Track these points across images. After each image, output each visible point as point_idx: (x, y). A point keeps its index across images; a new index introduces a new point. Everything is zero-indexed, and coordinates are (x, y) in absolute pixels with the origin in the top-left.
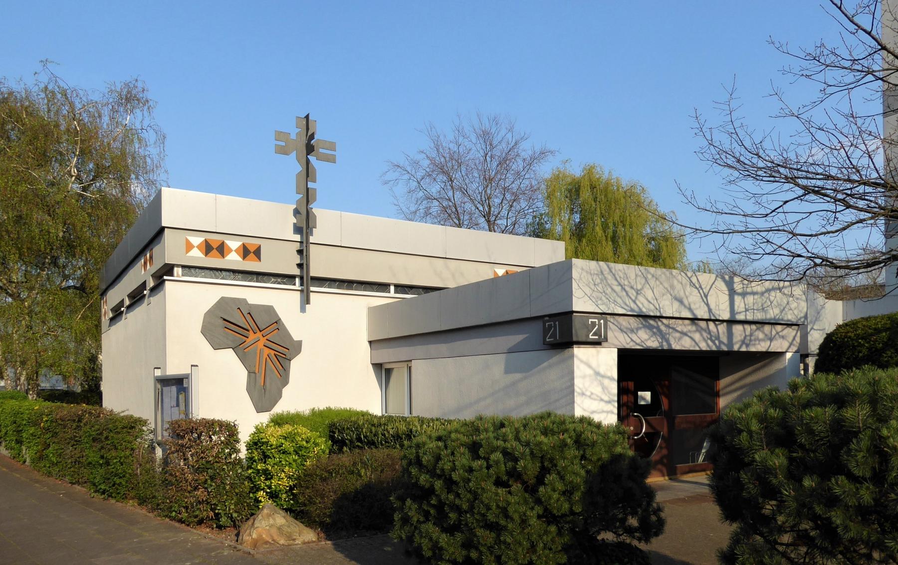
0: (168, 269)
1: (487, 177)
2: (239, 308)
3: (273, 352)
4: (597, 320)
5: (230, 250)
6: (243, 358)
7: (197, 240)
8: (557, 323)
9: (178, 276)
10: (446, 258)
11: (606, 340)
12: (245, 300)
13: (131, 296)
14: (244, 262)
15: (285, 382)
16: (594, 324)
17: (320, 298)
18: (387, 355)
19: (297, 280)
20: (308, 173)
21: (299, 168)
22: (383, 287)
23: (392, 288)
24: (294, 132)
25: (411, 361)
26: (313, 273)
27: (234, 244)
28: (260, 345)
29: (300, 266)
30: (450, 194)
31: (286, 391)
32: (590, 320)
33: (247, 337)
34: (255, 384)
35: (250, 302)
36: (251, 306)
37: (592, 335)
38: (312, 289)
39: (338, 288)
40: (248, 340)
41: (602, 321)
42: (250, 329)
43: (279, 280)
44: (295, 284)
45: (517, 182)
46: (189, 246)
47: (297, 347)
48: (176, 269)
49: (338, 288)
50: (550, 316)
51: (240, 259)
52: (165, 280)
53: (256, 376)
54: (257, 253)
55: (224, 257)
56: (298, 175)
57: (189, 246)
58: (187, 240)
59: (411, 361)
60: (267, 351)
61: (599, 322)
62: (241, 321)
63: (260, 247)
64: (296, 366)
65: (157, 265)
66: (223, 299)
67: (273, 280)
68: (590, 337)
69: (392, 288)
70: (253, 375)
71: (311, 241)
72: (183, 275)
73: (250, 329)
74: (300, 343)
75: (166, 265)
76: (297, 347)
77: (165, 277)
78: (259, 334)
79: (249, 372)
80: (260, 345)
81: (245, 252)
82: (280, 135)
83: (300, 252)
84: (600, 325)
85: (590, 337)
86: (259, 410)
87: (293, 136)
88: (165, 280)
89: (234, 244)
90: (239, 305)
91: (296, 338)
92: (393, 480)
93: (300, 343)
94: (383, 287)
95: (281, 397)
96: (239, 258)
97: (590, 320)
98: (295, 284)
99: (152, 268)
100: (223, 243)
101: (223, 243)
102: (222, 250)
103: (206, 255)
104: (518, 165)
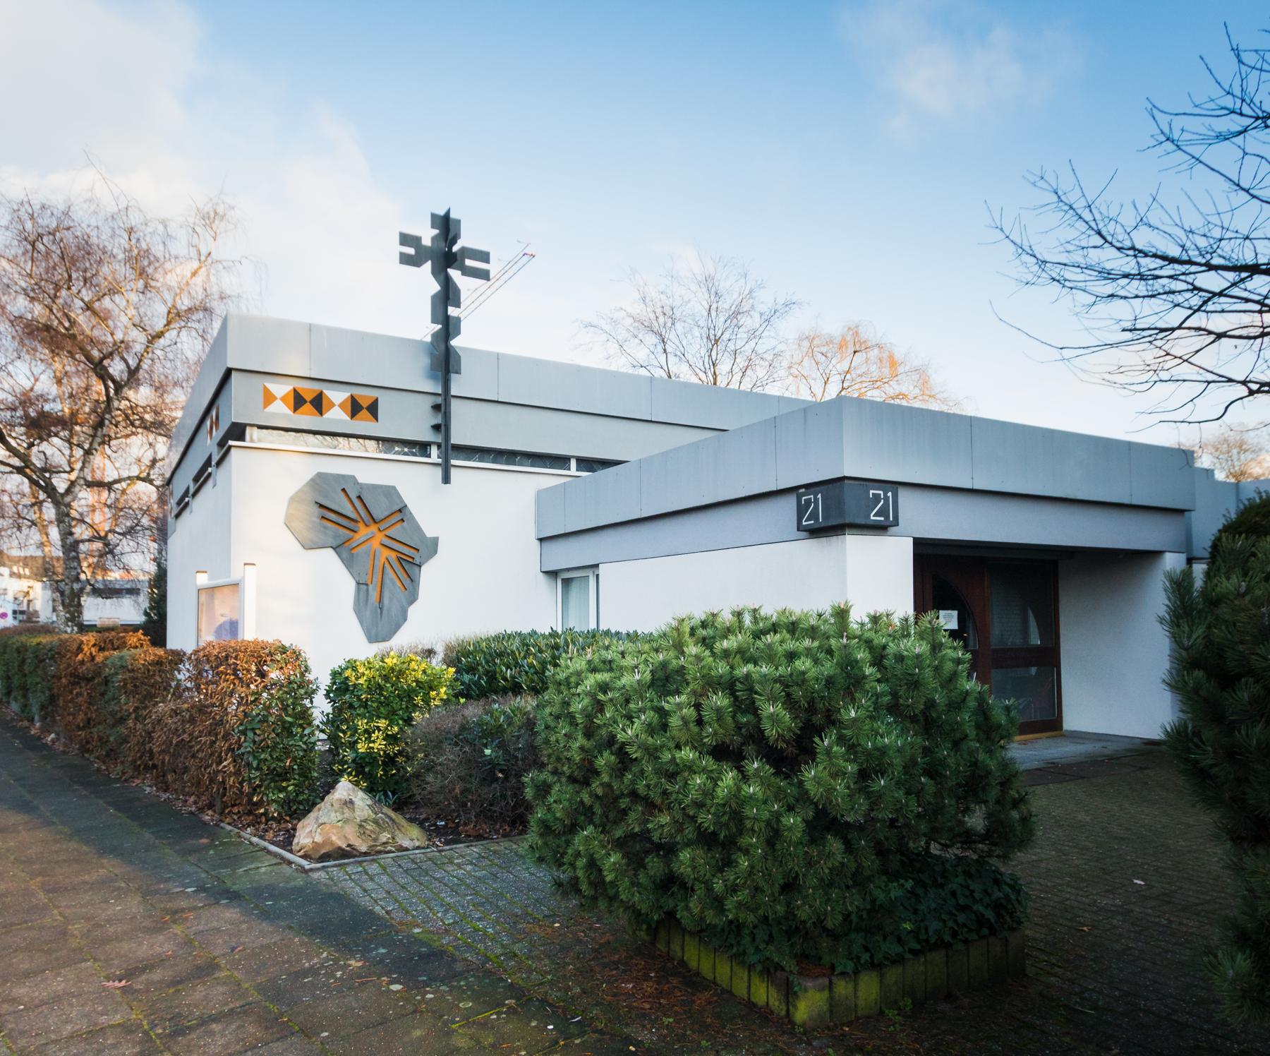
0: (237, 431)
1: (712, 337)
2: (344, 490)
3: (393, 555)
4: (881, 492)
5: (332, 405)
6: (349, 562)
7: (281, 389)
8: (819, 496)
9: (252, 441)
10: (651, 421)
11: (896, 523)
12: (353, 478)
13: (196, 479)
14: (353, 421)
15: (413, 598)
16: (877, 497)
17: (467, 476)
18: (567, 556)
19: (434, 451)
20: (448, 295)
21: (435, 287)
22: (559, 461)
23: (573, 463)
24: (428, 235)
25: (597, 566)
26: (455, 439)
27: (337, 396)
28: (375, 544)
29: (436, 428)
30: (662, 358)
31: (413, 611)
32: (871, 492)
33: (355, 532)
34: (367, 599)
35: (360, 480)
36: (362, 486)
37: (875, 515)
38: (453, 462)
39: (493, 462)
40: (357, 536)
41: (890, 494)
42: (359, 519)
43: (406, 450)
44: (429, 456)
45: (752, 344)
46: (269, 398)
47: (432, 546)
48: (248, 430)
49: (494, 462)
50: (807, 486)
51: (346, 418)
52: (230, 447)
53: (367, 590)
54: (373, 409)
55: (321, 414)
56: (434, 298)
57: (269, 398)
58: (265, 388)
59: (597, 566)
60: (386, 553)
61: (885, 494)
62: (348, 510)
63: (376, 400)
64: (429, 574)
65: (224, 427)
66: (320, 475)
67: (397, 449)
68: (872, 518)
69: (573, 463)
70: (365, 587)
71: (453, 393)
72: (260, 441)
73: (359, 519)
74: (435, 542)
75: (234, 425)
76: (432, 546)
77: (231, 443)
78: (373, 528)
79: (358, 583)
80: (375, 544)
81: (355, 408)
82: (406, 239)
83: (436, 408)
84: (886, 499)
85: (872, 518)
86: (373, 638)
87: (427, 242)
88: (230, 447)
89: (337, 396)
90: (345, 485)
91: (429, 533)
92: (1182, 711)
93: (435, 542)
94: (559, 461)
95: (405, 619)
96: (345, 417)
97: (871, 492)
98: (429, 456)
99: (218, 434)
100: (321, 393)
101: (321, 395)
102: (319, 404)
103: (295, 410)
104: (749, 322)
